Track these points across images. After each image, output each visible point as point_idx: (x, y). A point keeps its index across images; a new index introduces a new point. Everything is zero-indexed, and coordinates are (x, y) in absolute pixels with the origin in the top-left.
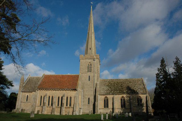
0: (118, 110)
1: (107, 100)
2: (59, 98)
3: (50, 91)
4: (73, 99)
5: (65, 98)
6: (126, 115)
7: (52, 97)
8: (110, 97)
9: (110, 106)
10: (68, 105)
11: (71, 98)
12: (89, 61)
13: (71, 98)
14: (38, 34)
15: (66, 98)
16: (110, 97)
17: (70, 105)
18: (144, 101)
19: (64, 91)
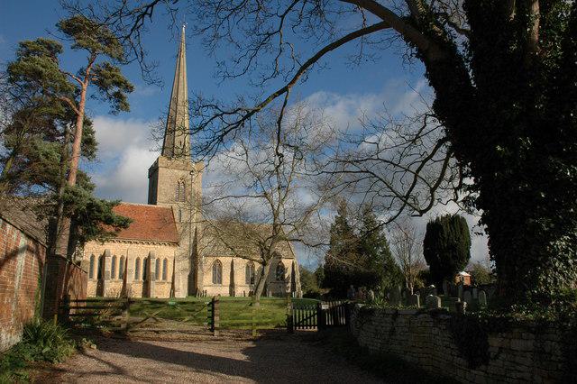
0: (242, 289)
1: (220, 266)
2: (138, 260)
3: (117, 244)
4: (170, 264)
5: (153, 261)
6: (84, 308)
7: (122, 258)
8: (226, 260)
9: (226, 279)
10: (161, 278)
11: (165, 261)
12: (181, 173)
13: (165, 261)
14: (377, 125)
15: (111, 258)
16: (226, 260)
17: (165, 278)
18: (288, 274)
19: (152, 246)
